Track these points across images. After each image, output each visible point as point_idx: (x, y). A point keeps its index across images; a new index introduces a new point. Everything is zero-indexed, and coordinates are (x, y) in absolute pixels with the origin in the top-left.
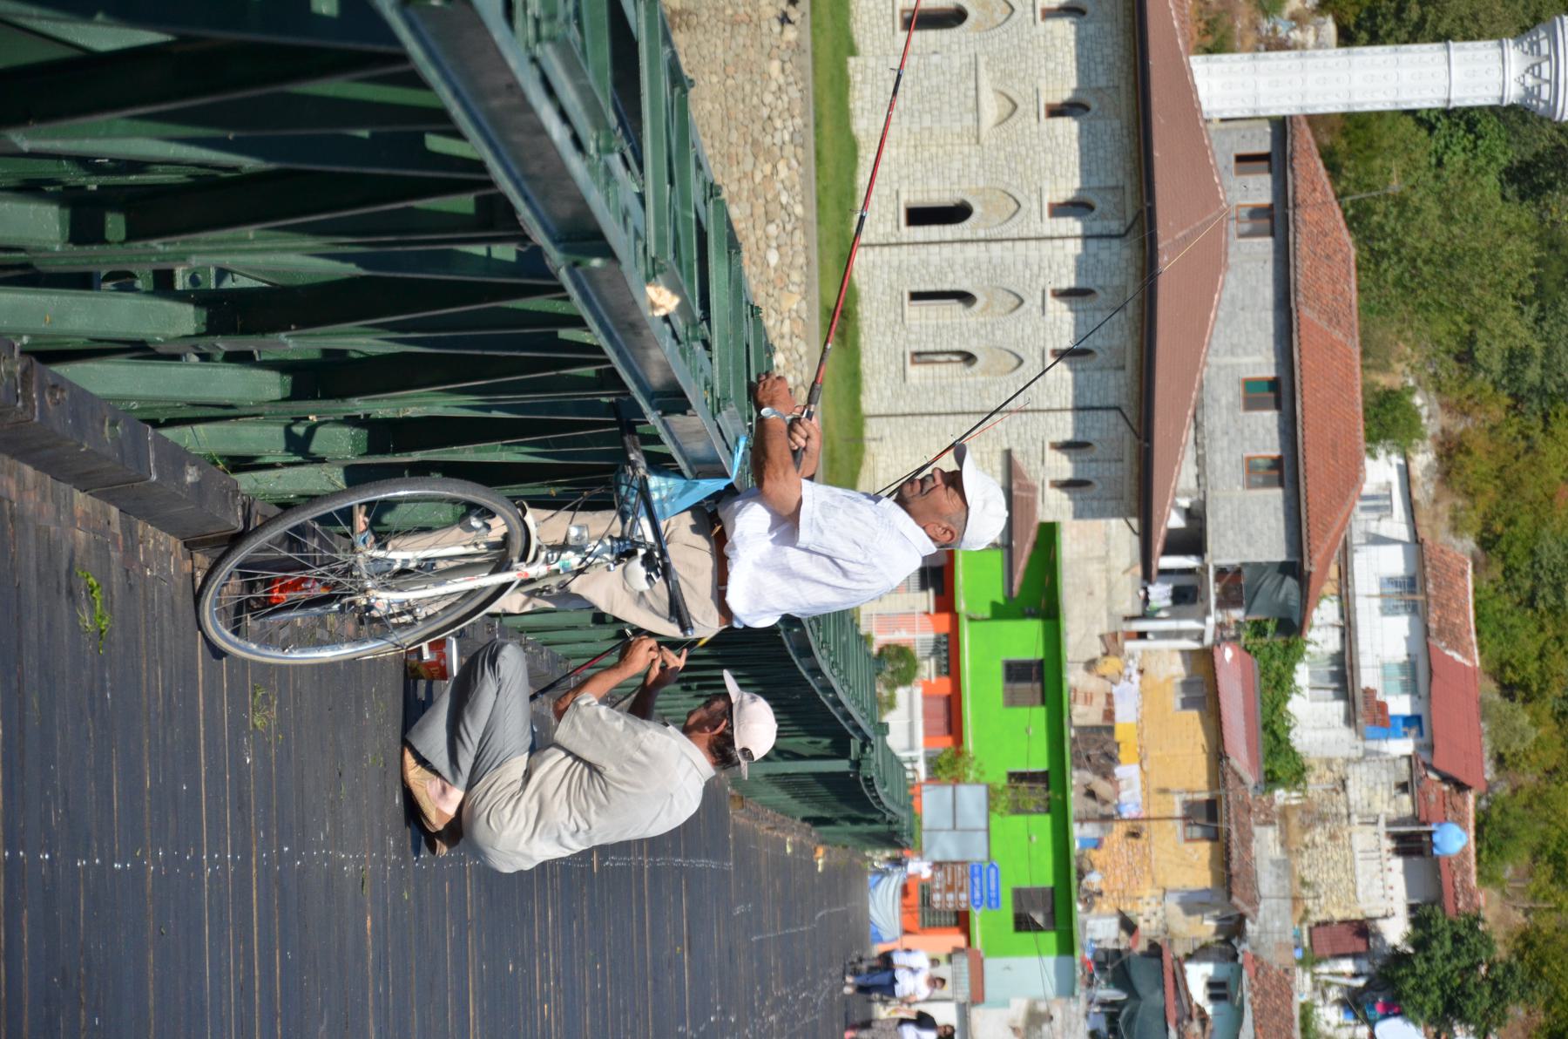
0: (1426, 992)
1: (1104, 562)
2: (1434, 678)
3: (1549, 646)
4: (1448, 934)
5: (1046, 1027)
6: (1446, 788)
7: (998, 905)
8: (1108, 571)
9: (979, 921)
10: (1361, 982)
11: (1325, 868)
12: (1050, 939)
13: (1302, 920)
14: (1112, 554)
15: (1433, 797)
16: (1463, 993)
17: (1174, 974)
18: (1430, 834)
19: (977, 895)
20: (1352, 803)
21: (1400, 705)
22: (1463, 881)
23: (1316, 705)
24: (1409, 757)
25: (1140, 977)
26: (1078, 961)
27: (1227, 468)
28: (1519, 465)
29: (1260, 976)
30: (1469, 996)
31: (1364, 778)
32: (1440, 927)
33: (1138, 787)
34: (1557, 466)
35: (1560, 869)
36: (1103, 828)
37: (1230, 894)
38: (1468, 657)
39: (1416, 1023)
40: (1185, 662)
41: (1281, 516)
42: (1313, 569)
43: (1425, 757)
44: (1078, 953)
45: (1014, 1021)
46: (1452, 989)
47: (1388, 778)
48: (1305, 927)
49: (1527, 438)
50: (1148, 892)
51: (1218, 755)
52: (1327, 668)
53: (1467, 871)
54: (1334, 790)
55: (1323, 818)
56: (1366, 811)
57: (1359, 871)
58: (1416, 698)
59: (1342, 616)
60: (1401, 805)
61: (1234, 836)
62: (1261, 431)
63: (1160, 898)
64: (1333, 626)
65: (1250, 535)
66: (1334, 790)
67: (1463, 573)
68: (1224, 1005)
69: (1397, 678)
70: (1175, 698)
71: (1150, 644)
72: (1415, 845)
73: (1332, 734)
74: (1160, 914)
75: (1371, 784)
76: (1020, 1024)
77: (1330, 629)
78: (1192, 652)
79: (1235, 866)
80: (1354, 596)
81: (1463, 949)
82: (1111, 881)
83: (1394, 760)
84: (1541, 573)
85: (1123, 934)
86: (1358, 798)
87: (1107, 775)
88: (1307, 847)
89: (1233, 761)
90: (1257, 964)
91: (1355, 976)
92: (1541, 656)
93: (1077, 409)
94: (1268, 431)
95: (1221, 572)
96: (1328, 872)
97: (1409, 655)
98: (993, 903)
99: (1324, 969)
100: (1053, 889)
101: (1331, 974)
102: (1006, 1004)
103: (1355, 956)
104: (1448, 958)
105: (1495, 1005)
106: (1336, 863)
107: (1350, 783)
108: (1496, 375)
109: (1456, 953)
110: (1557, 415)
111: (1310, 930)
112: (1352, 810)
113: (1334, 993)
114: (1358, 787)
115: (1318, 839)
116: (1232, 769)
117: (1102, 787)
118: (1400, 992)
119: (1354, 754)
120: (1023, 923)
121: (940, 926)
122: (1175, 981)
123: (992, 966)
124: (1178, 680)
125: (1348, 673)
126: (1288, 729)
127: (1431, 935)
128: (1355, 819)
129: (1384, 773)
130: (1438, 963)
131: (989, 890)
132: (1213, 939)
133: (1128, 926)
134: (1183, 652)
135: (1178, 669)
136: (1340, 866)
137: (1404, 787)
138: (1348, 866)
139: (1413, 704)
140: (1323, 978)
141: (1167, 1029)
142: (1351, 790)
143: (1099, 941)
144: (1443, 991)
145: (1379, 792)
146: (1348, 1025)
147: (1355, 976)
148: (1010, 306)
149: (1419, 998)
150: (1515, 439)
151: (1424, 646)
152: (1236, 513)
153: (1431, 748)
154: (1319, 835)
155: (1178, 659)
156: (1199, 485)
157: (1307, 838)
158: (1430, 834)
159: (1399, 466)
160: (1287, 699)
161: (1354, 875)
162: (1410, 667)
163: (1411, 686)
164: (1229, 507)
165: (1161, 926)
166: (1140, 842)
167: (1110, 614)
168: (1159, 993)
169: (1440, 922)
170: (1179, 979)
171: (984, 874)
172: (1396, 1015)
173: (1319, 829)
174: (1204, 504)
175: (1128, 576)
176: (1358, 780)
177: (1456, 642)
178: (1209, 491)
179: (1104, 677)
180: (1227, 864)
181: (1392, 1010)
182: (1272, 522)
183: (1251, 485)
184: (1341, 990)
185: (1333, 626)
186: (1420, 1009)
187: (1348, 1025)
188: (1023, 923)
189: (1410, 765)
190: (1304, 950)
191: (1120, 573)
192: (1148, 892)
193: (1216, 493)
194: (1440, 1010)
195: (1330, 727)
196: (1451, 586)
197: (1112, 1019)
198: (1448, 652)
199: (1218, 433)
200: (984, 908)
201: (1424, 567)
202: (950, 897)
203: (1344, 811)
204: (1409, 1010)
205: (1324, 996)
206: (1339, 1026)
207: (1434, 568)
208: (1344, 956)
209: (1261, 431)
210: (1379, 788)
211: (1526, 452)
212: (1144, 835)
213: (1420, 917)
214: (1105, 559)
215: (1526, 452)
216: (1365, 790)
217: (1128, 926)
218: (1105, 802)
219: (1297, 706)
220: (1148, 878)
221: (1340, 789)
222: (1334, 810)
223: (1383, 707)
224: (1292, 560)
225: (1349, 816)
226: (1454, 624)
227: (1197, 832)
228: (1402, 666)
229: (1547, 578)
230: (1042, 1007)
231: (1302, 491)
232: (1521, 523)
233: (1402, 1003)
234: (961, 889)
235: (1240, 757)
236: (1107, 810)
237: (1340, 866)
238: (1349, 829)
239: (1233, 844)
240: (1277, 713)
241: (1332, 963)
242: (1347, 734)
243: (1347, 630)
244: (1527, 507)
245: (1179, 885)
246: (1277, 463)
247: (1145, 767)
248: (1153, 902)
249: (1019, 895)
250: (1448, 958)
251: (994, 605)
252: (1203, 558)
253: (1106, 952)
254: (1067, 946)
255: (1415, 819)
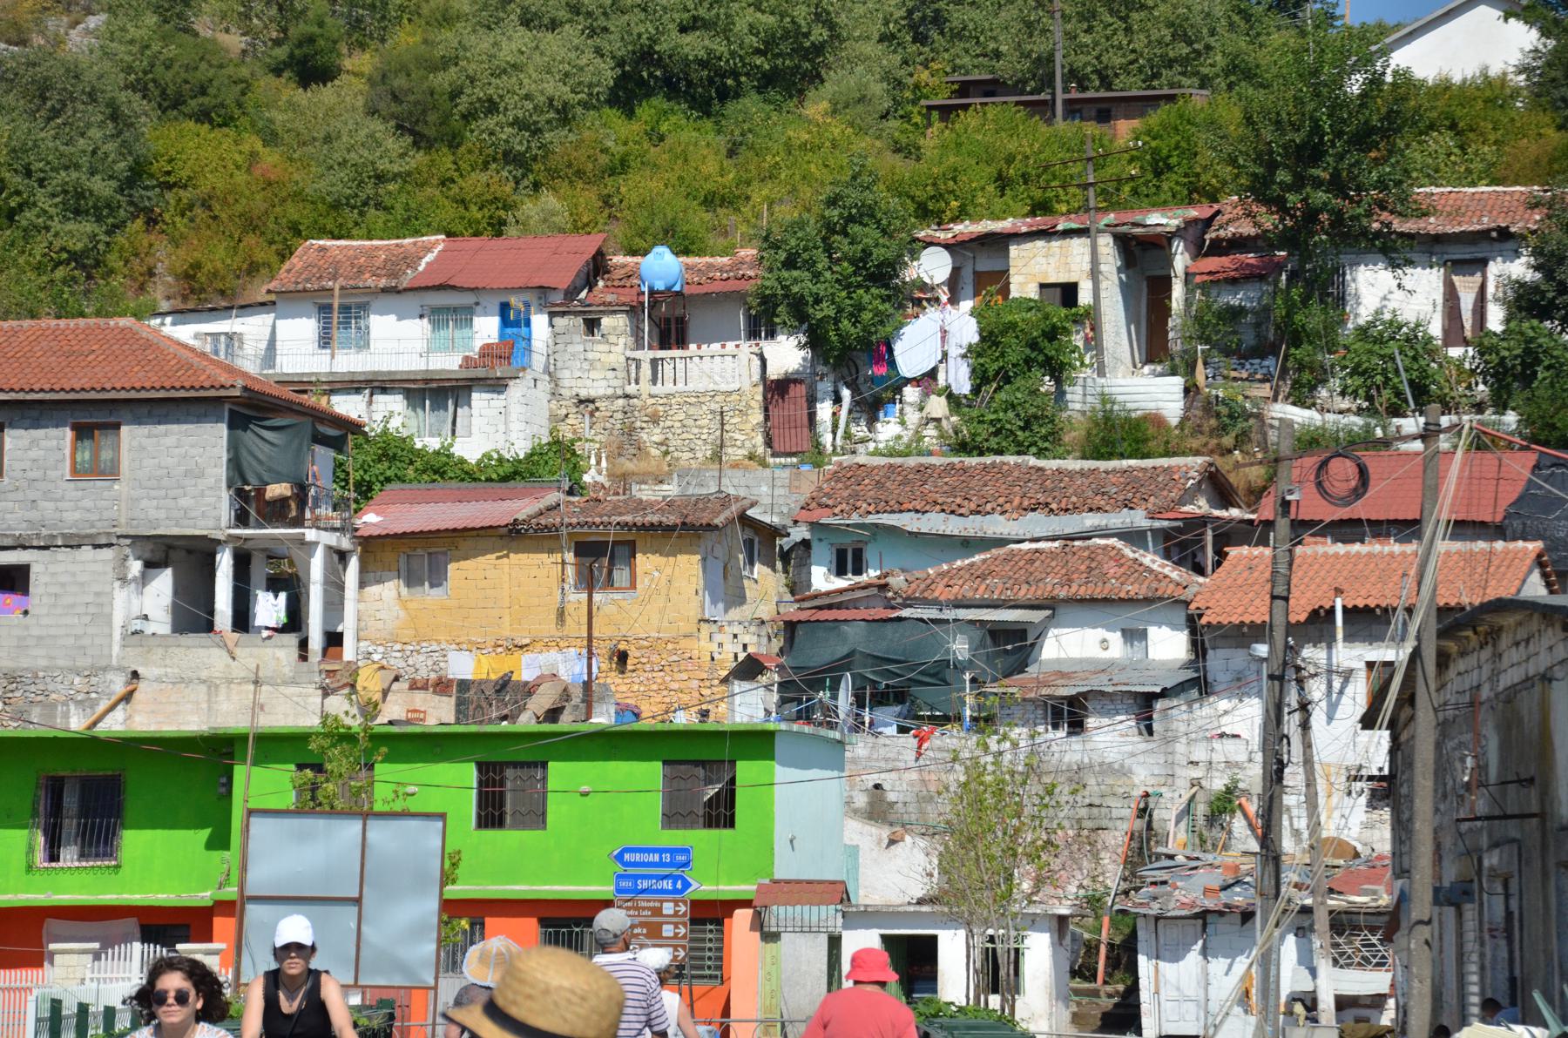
0: (860, 308)
1: (217, 686)
2: (451, 283)
3: (451, 193)
4: (785, 274)
5: (891, 797)
6: (601, 283)
7: (686, 851)
8: (230, 681)
9: (706, 887)
10: (846, 393)
11: (696, 431)
12: (746, 771)
13: (764, 465)
14: (204, 674)
15: (610, 298)
16: (861, 260)
17: (820, 608)
18: (652, 292)
19: (667, 885)
20: (610, 391)
21: (487, 328)
22: (721, 270)
23: (474, 430)
24: (552, 315)
25: (823, 652)
26: (783, 726)
27: (87, 503)
28: (224, 216)
29: (830, 502)
30: (867, 253)
31: (579, 374)
32: (776, 284)
33: (553, 656)
34: (231, 176)
35: (723, 199)
36: (602, 699)
37: (710, 527)
38: (431, 250)
39: (902, 325)
40: (380, 581)
41: (162, 428)
42: (240, 383)
43: (558, 298)
44: (771, 726)
45: (880, 841)
46: (855, 273)
47: (578, 341)
48: (771, 460)
49: (191, 207)
50: (703, 646)
51: (513, 536)
52: (427, 417)
53: (710, 266)
54: (592, 415)
55: (630, 431)
56: (622, 374)
57: (701, 387)
58: (478, 309)
59: (358, 391)
60: (615, 328)
61: (628, 518)
62: (33, 454)
63: (714, 628)
64: (370, 403)
65: (187, 473)
66: (592, 415)
67: (323, 249)
68: (870, 554)
69: (450, 331)
70: (429, 596)
71: (348, 628)
72: (673, 327)
73: (516, 410)
74: (737, 629)
75: (586, 366)
76: (885, 833)
77: (374, 407)
78: (363, 570)
79: (671, 519)
80: (331, 373)
81: (805, 256)
82: (686, 698)
83: (556, 335)
84: (363, 196)
85: (763, 679)
86: (604, 383)
87: (529, 690)
88: (666, 453)
89: (521, 516)
90: (814, 505)
91: (838, 400)
92: (463, 202)
93: (1157, 958)
94: (34, 443)
95: (242, 519)
96: (701, 427)
97: (421, 316)
98: (681, 858)
99: (827, 439)
100: (665, 763)
101: (834, 433)
102: (853, 851)
103: (812, 401)
104: (817, 276)
105: (878, 222)
106: (688, 416)
107: (583, 394)
108: (99, 230)
109: (810, 264)
110: (168, 173)
111: (774, 455)
112: (619, 392)
113: (860, 430)
114: (589, 383)
115: (656, 438)
116: (531, 517)
117: (542, 701)
118: (858, 339)
119: (545, 386)
120: (721, 813)
121: (720, 949)
122: (830, 607)
123: (787, 867)
124: (404, 591)
125: (434, 385)
126: (501, 460)
127: (786, 296)
128: (631, 389)
129: (570, 349)
130: (820, 289)
131: (661, 864)
132: (781, 576)
133: (749, 669)
134: (362, 584)
135: (388, 592)
136: (692, 410)
137: (592, 325)
138: (693, 400)
139: (486, 314)
140: (839, 442)
141: (899, 619)
142: (593, 393)
143: (768, 712)
144: (859, 286)
145: (598, 356)
146: (902, 410)
147: (838, 400)
148: (1199, 928)
149: (866, 316)
150: (192, 220)
151: (410, 294)
152: (153, 493)
153: (543, 290)
154: (651, 436)
155: (373, 590)
156: (110, 545)
157: (654, 452)
158: (652, 292)
159: (174, 324)
160: (462, 461)
161: (704, 394)
162: (438, 316)
163: (463, 316)
164: (144, 503)
165: (753, 629)
166: (633, 653)
167: (293, 682)
168: (845, 628)
169: (767, 283)
170: (827, 601)
171: (632, 871)
172: (890, 351)
173: (644, 436)
174: (136, 539)
175: (238, 652)
176: (579, 383)
177: (411, 260)
178: (119, 531)
179: (385, 693)
180: (669, 529)
181: (883, 352)
182: (170, 441)
183: (111, 472)
184: (856, 421)
185: (370, 403)
186: (882, 317)
187: (902, 410)
188: (721, 813)
189: (563, 314)
190: (802, 462)
191: (234, 664)
192: (703, 646)
193: (123, 520)
194: (884, 292)
195: (504, 412)
196: (337, 264)
197: (880, 699)
198: (421, 269)
199: (33, 515)
200: (688, 874)
201: (305, 290)
202: (668, 930)
203: (621, 402)
204: (883, 331)
205: (863, 441)
206: (902, 423)
207: (308, 280)
208: (812, 417)
209: (33, 454)
210: (590, 355)
211: (210, 208)
212: (622, 647)
213: (761, 325)
214: (211, 685)
215: (210, 208)
216: (593, 375)
217: (749, 669)
218: (566, 695)
219: (469, 449)
220: (683, 643)
221: (591, 407)
222: (619, 415)
223: (486, 351)
224: (226, 414)
225: (627, 396)
226: (386, 261)
227: (621, 576)
228: (436, 325)
229: (369, 190)
230: (861, 800)
231: (123, 395)
232: (296, 217)
233: (874, 338)
234: (657, 912)
235: (522, 508)
236: (577, 694)
237: (692, 410)
238: (644, 396)
239: (639, 520)
240: (477, 475)
241: (820, 429)
242: (516, 390)
243: (378, 385)
244: (278, 209)
245: (696, 600)
246: (83, 432)
247: (527, 641)
248: (718, 638)
249: (671, 819)
250: (817, 276)
251: (212, 845)
252: (218, 542)
253: (783, 701)
254: (758, 742)
255: (634, 311)
